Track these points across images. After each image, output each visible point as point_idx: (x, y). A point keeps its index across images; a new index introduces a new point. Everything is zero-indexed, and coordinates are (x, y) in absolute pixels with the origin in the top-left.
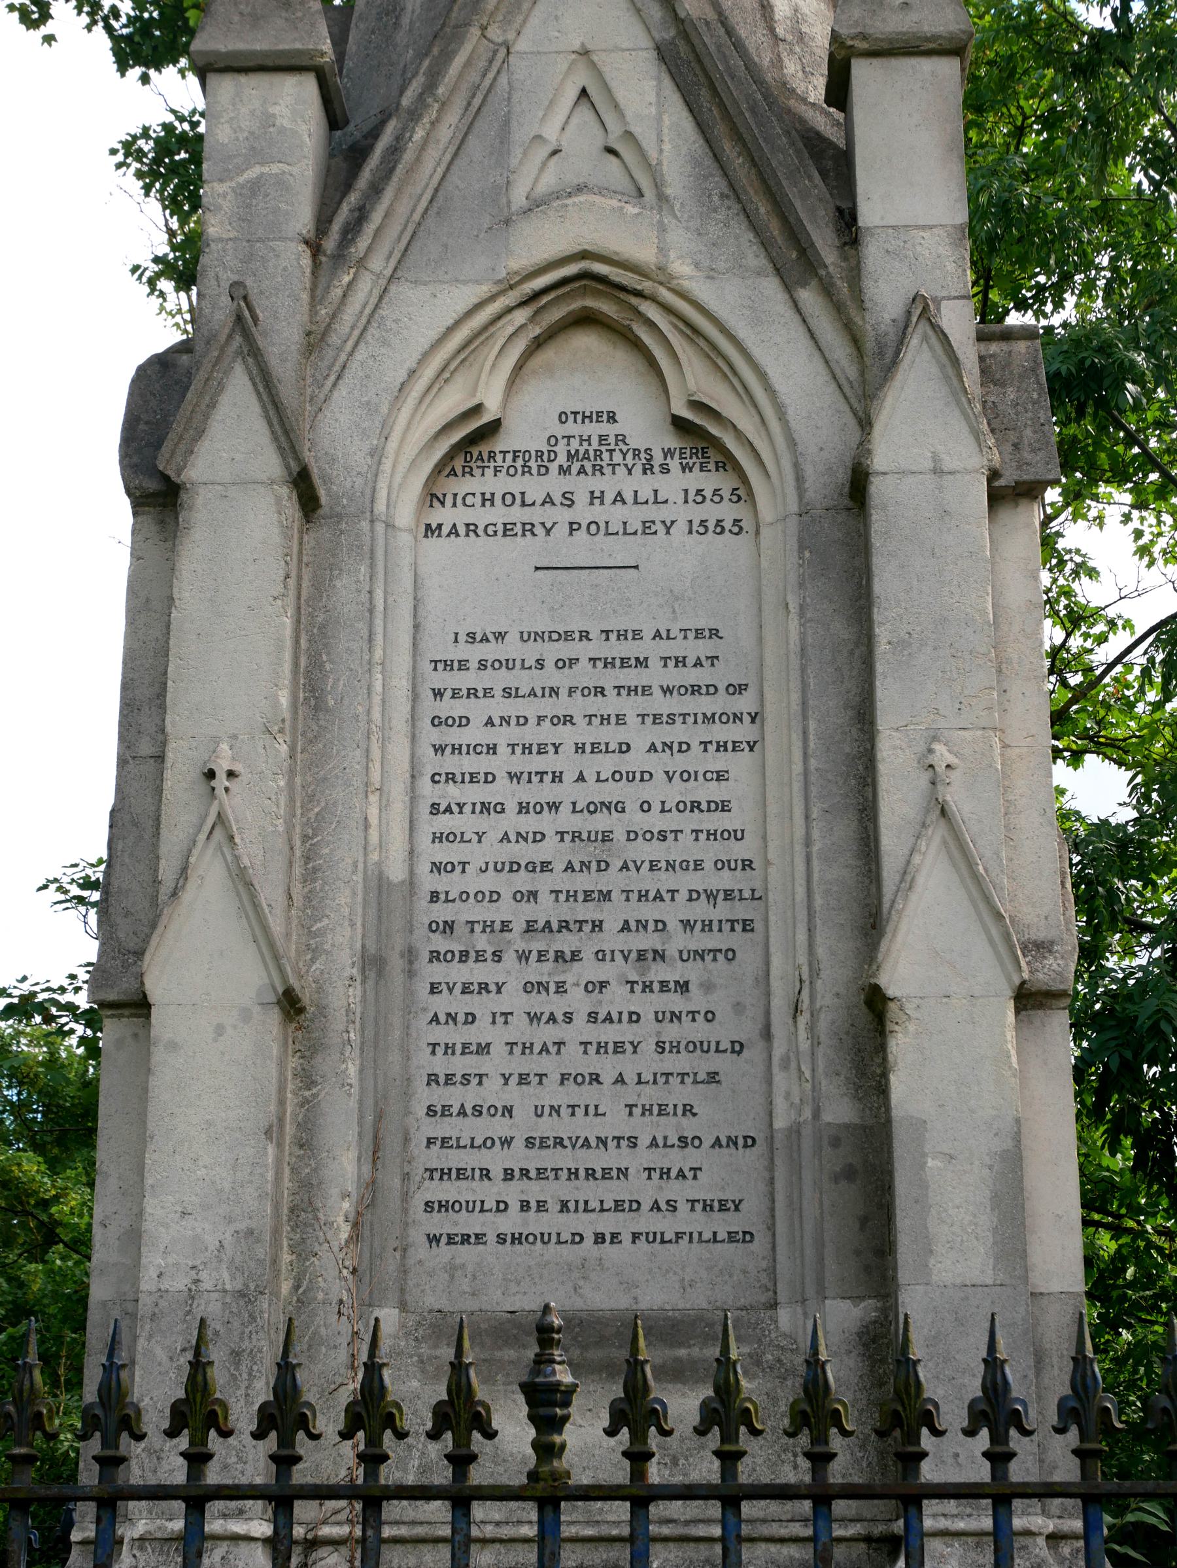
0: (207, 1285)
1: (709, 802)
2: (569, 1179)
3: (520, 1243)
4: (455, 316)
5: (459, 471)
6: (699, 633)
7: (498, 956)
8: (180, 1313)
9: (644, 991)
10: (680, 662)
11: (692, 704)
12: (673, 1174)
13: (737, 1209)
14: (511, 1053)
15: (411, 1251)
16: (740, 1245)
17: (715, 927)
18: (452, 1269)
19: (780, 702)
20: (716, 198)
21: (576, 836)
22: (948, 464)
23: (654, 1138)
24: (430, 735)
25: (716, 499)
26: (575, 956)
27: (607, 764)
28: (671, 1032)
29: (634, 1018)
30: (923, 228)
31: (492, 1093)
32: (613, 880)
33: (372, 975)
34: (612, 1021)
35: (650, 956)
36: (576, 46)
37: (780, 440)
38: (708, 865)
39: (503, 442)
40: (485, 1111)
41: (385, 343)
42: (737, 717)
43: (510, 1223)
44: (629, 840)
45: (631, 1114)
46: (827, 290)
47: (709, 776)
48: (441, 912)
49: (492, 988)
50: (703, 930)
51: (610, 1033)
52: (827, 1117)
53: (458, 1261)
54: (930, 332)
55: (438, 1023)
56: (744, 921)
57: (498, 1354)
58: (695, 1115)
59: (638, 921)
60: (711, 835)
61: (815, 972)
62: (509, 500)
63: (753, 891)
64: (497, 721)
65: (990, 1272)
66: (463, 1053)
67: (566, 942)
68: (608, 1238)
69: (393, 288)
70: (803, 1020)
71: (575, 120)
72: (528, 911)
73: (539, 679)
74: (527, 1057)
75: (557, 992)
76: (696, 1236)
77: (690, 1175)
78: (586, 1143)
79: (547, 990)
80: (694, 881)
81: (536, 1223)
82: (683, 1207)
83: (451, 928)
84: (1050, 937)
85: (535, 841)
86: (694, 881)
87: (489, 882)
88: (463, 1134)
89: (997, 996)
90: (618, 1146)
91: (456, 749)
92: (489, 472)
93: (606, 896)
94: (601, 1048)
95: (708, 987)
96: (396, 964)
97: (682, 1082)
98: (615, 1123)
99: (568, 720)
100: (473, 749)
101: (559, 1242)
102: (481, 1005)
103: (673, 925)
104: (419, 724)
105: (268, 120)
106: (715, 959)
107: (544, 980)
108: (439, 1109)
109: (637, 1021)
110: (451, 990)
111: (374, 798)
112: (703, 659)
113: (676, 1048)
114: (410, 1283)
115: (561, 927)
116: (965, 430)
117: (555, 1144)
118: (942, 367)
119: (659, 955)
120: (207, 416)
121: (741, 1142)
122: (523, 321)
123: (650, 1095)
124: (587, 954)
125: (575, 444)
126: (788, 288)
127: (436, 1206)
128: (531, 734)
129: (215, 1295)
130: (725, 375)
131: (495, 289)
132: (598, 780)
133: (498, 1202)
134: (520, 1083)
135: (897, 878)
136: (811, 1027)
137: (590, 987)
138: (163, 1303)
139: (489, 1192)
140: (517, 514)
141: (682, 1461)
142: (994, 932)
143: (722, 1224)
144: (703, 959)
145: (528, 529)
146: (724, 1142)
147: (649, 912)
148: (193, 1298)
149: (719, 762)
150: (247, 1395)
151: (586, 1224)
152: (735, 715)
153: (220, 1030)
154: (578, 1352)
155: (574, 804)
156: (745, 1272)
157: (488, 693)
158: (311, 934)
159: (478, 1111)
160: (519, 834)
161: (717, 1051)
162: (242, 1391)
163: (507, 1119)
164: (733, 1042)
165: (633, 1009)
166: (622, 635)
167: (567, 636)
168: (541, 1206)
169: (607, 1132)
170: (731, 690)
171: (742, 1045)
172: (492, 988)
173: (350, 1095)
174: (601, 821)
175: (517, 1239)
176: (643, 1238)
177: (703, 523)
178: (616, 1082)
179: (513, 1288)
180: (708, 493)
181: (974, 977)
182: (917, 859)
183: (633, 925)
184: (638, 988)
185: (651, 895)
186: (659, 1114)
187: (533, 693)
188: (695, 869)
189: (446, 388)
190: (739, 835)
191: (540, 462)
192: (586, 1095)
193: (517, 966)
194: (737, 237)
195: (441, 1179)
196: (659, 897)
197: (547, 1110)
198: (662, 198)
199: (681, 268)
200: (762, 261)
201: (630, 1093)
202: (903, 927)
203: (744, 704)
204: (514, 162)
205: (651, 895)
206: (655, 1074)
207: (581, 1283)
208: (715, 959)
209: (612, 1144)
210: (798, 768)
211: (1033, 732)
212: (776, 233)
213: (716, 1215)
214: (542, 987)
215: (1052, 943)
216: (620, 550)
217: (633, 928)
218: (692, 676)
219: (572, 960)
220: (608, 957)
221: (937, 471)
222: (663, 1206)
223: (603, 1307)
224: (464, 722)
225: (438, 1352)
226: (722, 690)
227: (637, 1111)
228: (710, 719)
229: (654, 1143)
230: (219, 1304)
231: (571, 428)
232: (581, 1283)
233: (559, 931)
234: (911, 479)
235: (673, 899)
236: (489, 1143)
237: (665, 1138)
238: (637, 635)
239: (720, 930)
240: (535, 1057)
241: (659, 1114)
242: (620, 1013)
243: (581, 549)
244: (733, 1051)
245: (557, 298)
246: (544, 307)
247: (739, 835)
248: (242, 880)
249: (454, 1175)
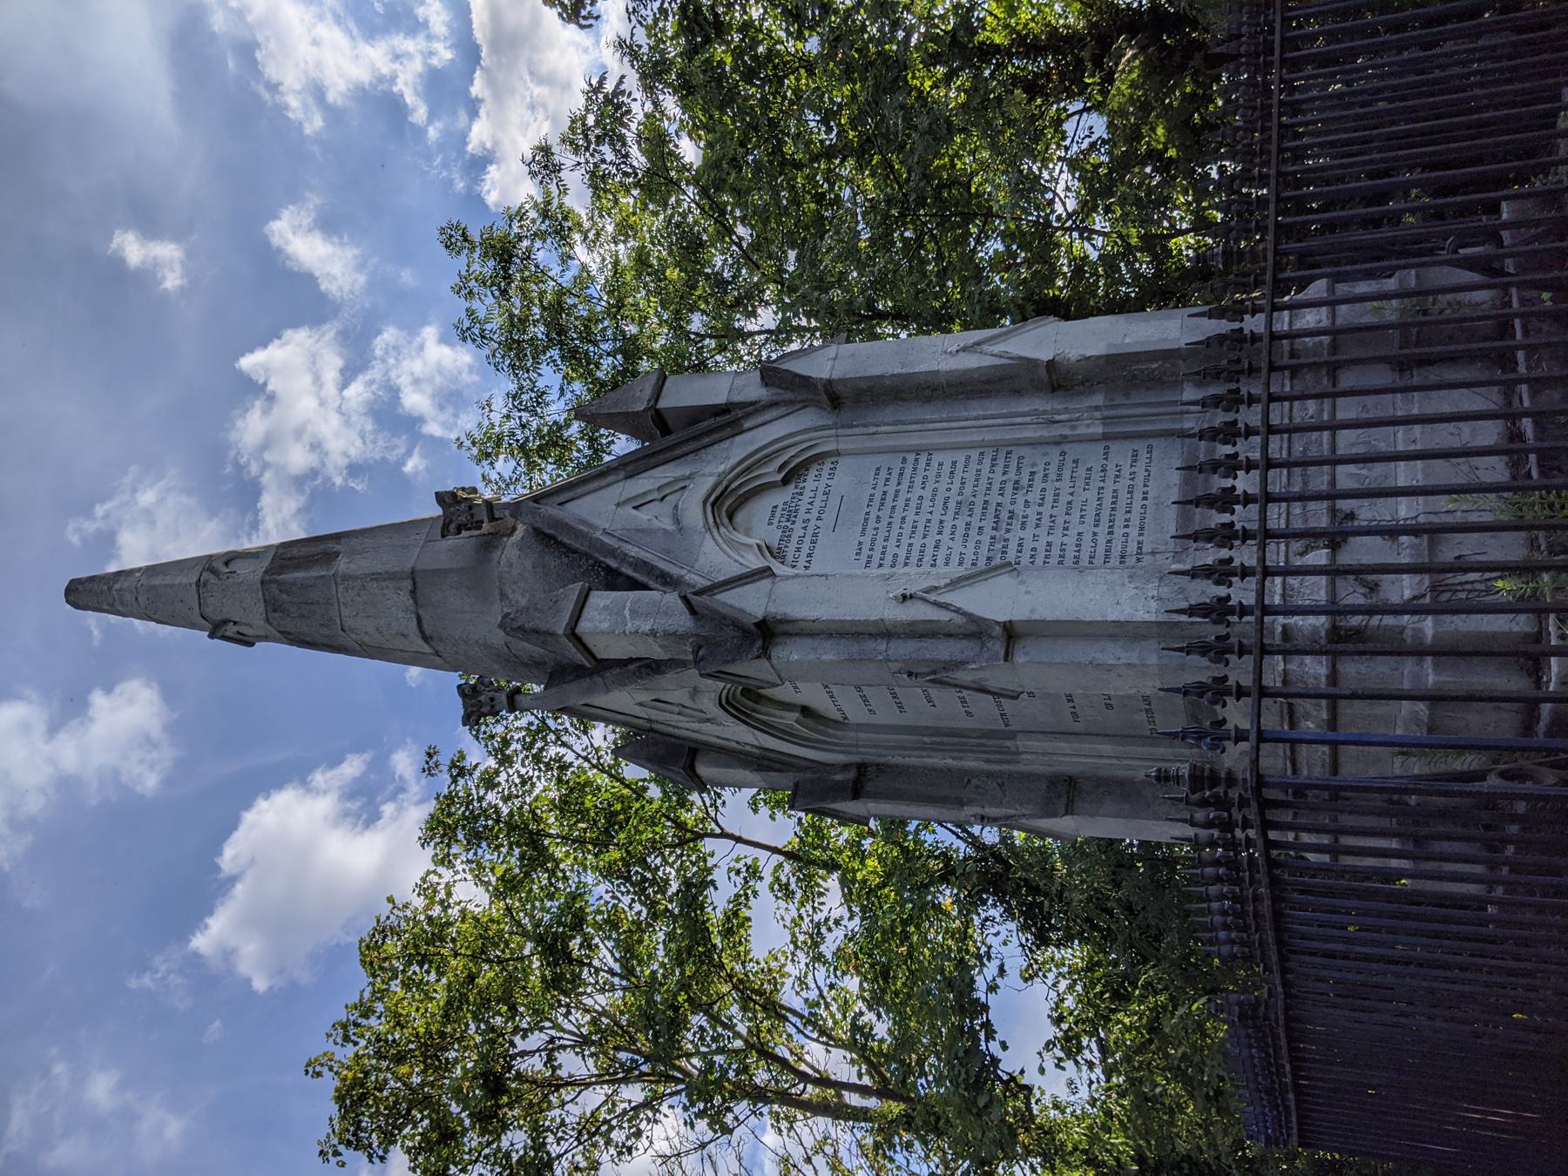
0: (1155, 593)
28: (1052, 476)
31: (1071, 540)
32: (979, 501)
46: (747, 416)
61: (1035, 413)
62: (801, 542)
67: (1004, 515)
81: (1135, 519)
87: (971, 544)
98: (1092, 495)
100: (909, 552)
123: (1080, 483)
140: (808, 539)
145: (815, 535)
153: (1028, 592)
174: (952, 505)
175: (1142, 528)
199: (722, 468)
224: (895, 556)
231: (775, 521)
243: (829, 517)
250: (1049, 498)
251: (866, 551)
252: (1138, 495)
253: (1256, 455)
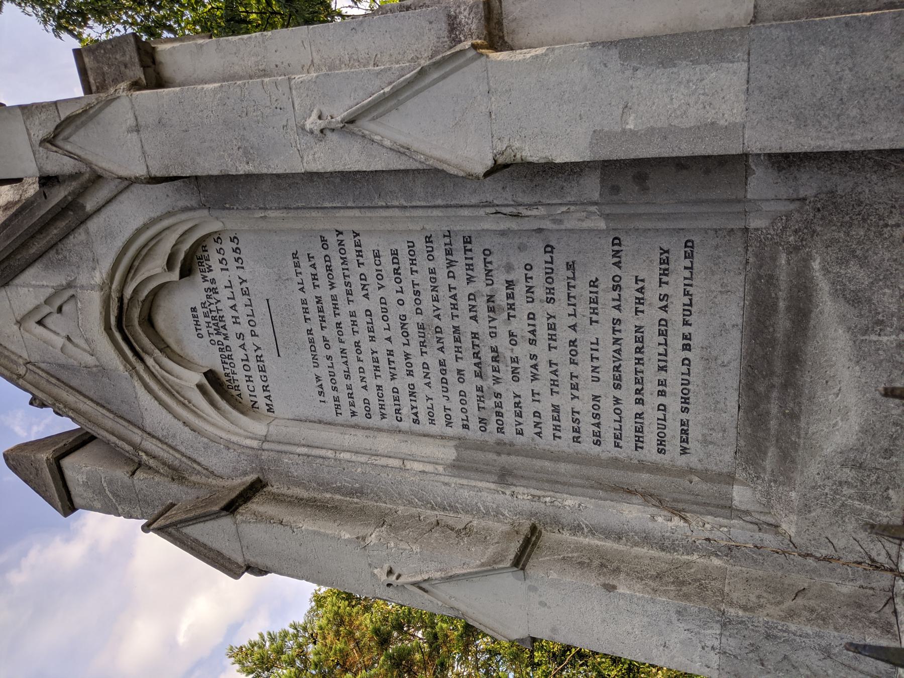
1: (393, 263)
2: (643, 364)
3: (688, 399)
4: (153, 400)
5: (238, 392)
6: (297, 265)
7: (498, 395)
8: (736, 661)
9: (514, 309)
10: (315, 277)
11: (338, 271)
12: (640, 296)
13: (667, 252)
14: (557, 393)
15: (692, 465)
16: (695, 250)
17: (470, 262)
18: (705, 442)
19: (322, 222)
20: (60, 257)
21: (422, 344)
22: (131, 122)
23: (614, 307)
24: (376, 420)
25: (222, 252)
26: (494, 350)
27: (379, 324)
28: (540, 293)
29: (531, 316)
30: (29, 134)
31: (584, 406)
32: (447, 324)
33: (510, 480)
34: (535, 330)
35: (491, 304)
36: (16, 327)
37: (184, 216)
38: (431, 265)
39: (219, 368)
40: (596, 412)
41: (174, 436)
42: (341, 243)
43: (674, 404)
44: (421, 314)
45: (597, 322)
46: (84, 190)
47: (378, 262)
48: (474, 424)
49: (517, 400)
50: (472, 270)
51: (543, 332)
52: (596, 196)
53: (700, 438)
54: (61, 137)
55: (541, 433)
56: (464, 243)
57: (773, 432)
58: (597, 280)
59: (470, 311)
60: (413, 262)
61: (489, 204)
62: (247, 368)
63: (445, 236)
64: (364, 384)
65: (735, 66)
66: (559, 421)
67: (486, 355)
68: (686, 342)
69: (148, 430)
70: (525, 212)
71: (53, 328)
72: (469, 375)
73: (338, 360)
74: (560, 383)
75: (518, 362)
76: (687, 282)
77: (641, 284)
78: (618, 351)
79: (516, 368)
80: (442, 274)
81: (674, 387)
82: (665, 290)
83: (483, 419)
84: (445, 19)
85: (428, 368)
86: (442, 274)
87: (455, 398)
88: (612, 426)
89: (487, 70)
90: (619, 331)
91: (382, 407)
92: (235, 377)
93: (456, 329)
94: (552, 338)
95: (509, 268)
96: (504, 460)
97: (574, 287)
99: (357, 344)
100: (381, 397)
101: (689, 374)
102: (528, 408)
103: (470, 289)
104: (371, 426)
105: (85, 484)
106: (490, 263)
107: (510, 369)
108: (596, 438)
109: (534, 314)
110: (520, 424)
111: (409, 465)
112: (311, 263)
113: (550, 291)
114: (714, 468)
115: (477, 357)
116: (108, 110)
117: (618, 371)
118: (78, 128)
119: (490, 299)
120: (211, 549)
121: (616, 248)
122: (152, 360)
123: (583, 309)
124: (493, 343)
125: (211, 331)
126: (89, 216)
127: (661, 447)
128: (369, 366)
129: (724, 640)
130: (150, 250)
131: (136, 378)
132: (389, 329)
133: (659, 410)
134: (577, 389)
135: (403, 157)
136: (530, 206)
137: (513, 342)
138: (728, 669)
139: (651, 416)
140: (253, 364)
141: (880, 317)
142: (435, 75)
143: (678, 263)
144: (491, 271)
146: (617, 260)
147: (464, 304)
148: (725, 653)
149: (369, 257)
150: (800, 636)
151: (676, 355)
152: (339, 245)
153: (543, 604)
154: (776, 379)
155: (404, 344)
156: (717, 247)
157: (349, 387)
158: (487, 513)
159: (596, 416)
160: (425, 377)
161: (552, 263)
162: (798, 639)
163: (602, 400)
164: (546, 252)
165: (526, 317)
166: (306, 311)
167: (312, 341)
168: (662, 383)
169: (610, 337)
170: (325, 246)
171: (548, 246)
172: (517, 400)
173: (586, 507)
174: (413, 329)
175: (686, 400)
176: (687, 318)
177: (237, 260)
178: (575, 330)
179: (721, 405)
180: (221, 257)
181: (473, 91)
182: (387, 143)
183: (473, 314)
184: (512, 313)
185: (453, 302)
186: (597, 303)
187: (346, 363)
188: (435, 273)
189: (194, 401)
190: (411, 244)
191: (226, 359)
192: (584, 350)
193: (503, 384)
194: (74, 245)
195: (642, 442)
196: (454, 297)
197: (595, 374)
198: (70, 285)
199: (99, 277)
200: (81, 230)
201: (583, 321)
202: (437, 154)
203: (332, 240)
204: (75, 363)
205: (453, 302)
206: (569, 305)
207: (719, 362)
208: (490, 263)
209: (618, 335)
210: (357, 213)
211: (300, 42)
212: (64, 224)
213: (671, 266)
214: (514, 371)
215: (449, 16)
216: (261, 309)
217: (475, 314)
218: (321, 271)
219: (497, 352)
220: (494, 330)
221: (137, 129)
222: (664, 303)
223: (738, 348)
225: (769, 469)
226: (326, 252)
227: (595, 317)
228: (344, 261)
229: (618, 308)
230: (730, 639)
231: (204, 331)
232: (719, 362)
233: (480, 358)
234: (146, 148)
235: (455, 288)
236: (618, 412)
237: (614, 300)
238: (304, 302)
239: (472, 259)
240: (560, 379)
241: (597, 303)
242: (529, 325)
243: (265, 330)
244: (552, 252)
245: (136, 342)
246: (142, 349)
247: (411, 244)
249: (640, 434)
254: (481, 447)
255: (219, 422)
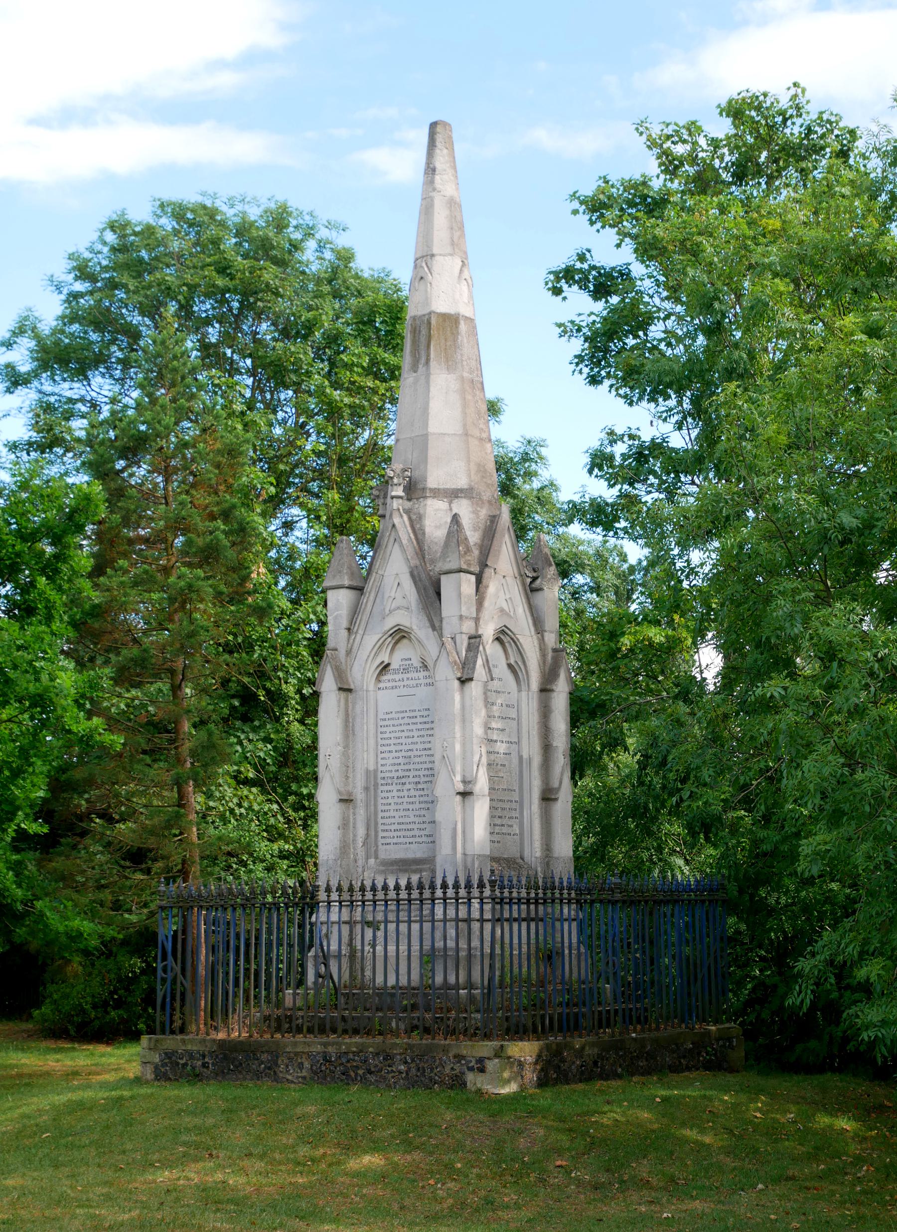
28: (421, 799)
31: (392, 814)
32: (411, 767)
39: (391, 667)
43: (395, 840)
48: (383, 775)
67: (403, 780)
81: (400, 840)
87: (390, 768)
98: (412, 819)
102: (389, 795)
123: (418, 813)
140: (394, 684)
151: (408, 840)
174: (409, 753)
191: (397, 671)
243: (405, 691)
248: (332, 778)
250: (411, 800)
251: (387, 717)
252: (411, 840)
253: (401, 897)
254: (376, 777)
255: (372, 670)
